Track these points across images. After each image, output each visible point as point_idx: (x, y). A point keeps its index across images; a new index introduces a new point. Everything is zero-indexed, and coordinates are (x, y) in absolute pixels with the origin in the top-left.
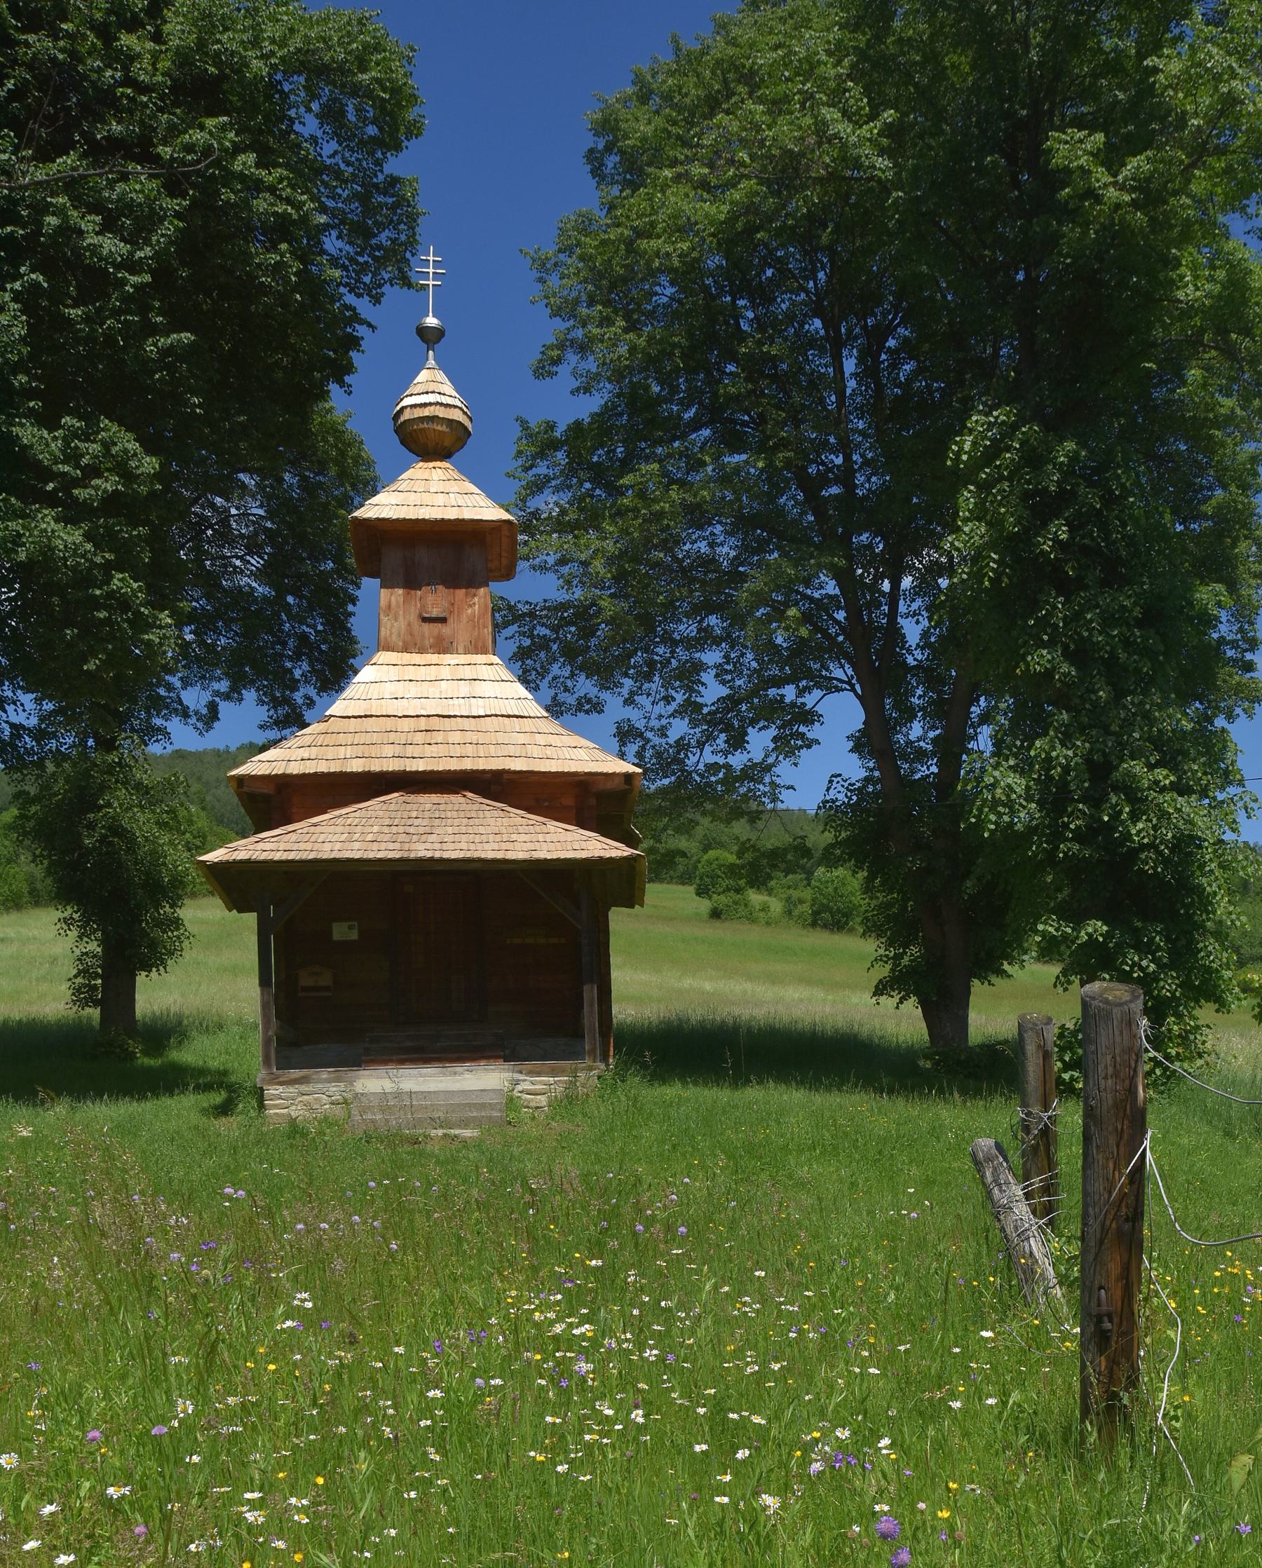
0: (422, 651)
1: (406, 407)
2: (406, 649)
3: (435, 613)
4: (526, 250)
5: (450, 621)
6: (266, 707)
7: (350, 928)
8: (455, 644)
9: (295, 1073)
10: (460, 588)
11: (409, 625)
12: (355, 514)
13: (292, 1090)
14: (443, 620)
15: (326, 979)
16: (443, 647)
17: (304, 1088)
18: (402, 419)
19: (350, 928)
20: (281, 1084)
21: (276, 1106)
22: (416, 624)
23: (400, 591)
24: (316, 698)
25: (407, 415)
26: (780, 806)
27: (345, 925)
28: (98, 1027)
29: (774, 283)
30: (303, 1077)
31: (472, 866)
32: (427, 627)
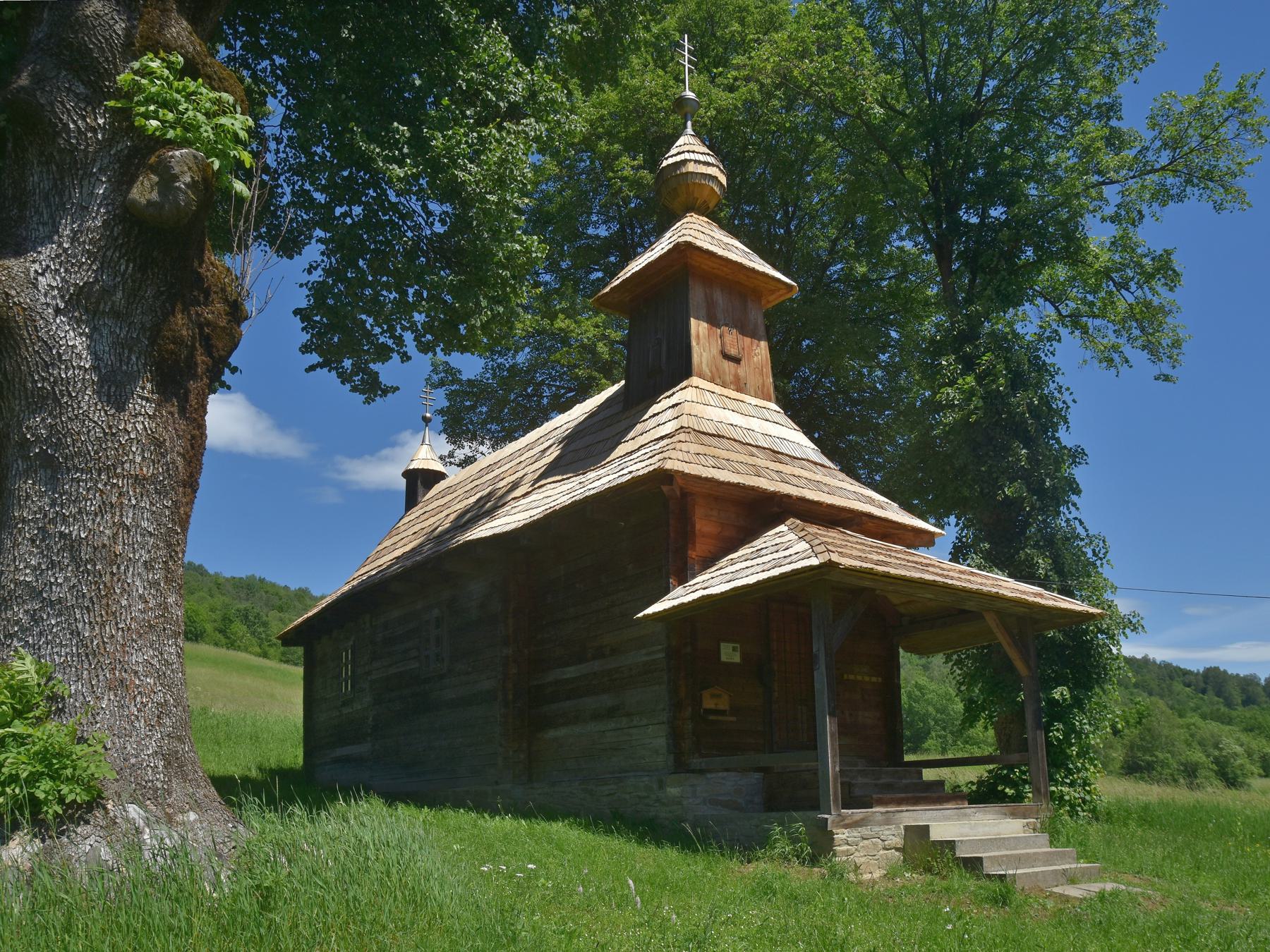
1: (690, 160)
2: (712, 381)
3: (733, 352)
5: (742, 362)
9: (858, 813)
14: (737, 360)
15: (723, 704)
17: (865, 831)
18: (684, 170)
19: (734, 649)
20: (846, 826)
23: (705, 325)
25: (691, 167)
30: (863, 819)
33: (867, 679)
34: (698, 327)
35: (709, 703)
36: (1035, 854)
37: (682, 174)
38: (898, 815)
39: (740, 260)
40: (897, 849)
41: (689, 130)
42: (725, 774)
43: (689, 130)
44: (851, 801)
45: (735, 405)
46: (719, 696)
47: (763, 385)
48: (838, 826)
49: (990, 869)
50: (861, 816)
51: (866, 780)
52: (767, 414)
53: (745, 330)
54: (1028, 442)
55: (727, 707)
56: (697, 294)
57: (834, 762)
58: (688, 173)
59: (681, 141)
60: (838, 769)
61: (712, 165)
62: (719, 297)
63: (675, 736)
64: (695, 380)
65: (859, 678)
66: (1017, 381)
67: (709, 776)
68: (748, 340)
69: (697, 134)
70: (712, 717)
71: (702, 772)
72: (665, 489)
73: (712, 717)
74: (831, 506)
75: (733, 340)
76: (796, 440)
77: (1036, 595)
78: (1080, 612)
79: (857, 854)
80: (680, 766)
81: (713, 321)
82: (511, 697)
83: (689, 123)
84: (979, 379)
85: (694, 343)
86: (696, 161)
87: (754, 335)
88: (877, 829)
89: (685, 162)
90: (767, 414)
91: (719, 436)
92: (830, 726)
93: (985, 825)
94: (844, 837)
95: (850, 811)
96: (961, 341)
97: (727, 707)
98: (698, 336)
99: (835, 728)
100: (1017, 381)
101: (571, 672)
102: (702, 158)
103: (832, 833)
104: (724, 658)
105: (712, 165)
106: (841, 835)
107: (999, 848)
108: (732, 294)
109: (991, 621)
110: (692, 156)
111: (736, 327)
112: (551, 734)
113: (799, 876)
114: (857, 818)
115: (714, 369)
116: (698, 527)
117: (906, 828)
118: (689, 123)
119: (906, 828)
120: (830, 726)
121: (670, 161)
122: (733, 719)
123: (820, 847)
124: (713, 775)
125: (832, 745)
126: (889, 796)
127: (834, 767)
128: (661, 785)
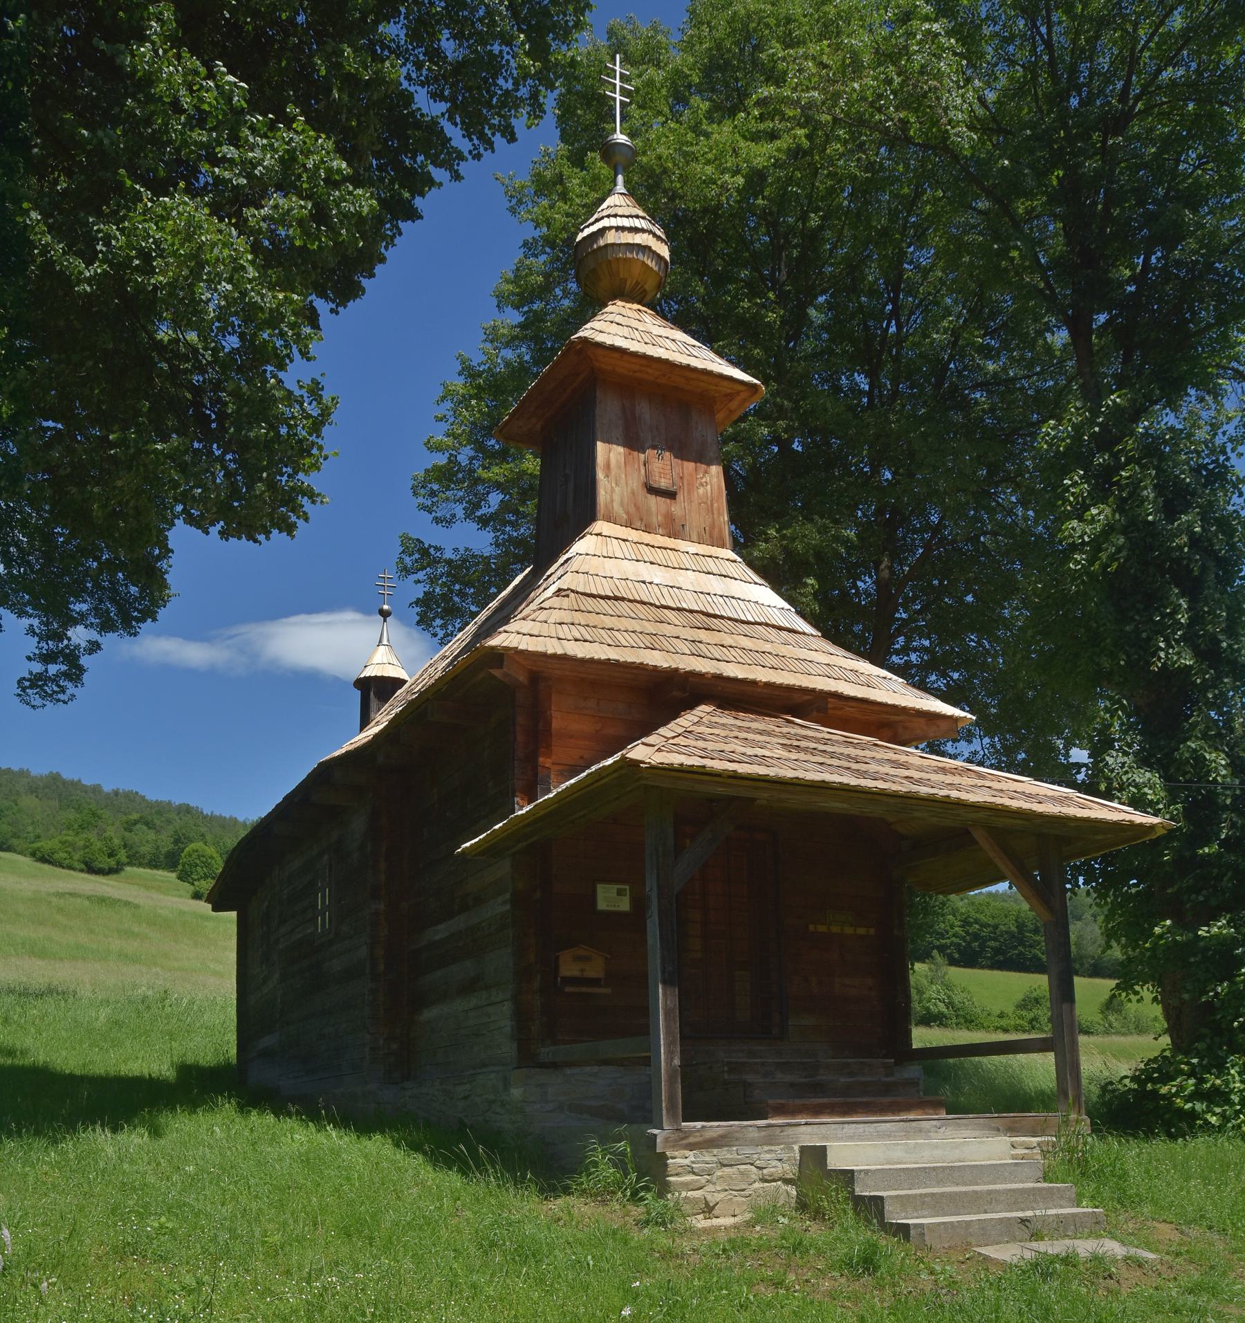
0: (648, 530)
1: (610, 228)
2: (629, 524)
3: (664, 483)
4: (499, 175)
5: (680, 497)
6: (36, 639)
7: (620, 893)
8: (687, 528)
9: (716, 1128)
10: (689, 460)
11: (633, 493)
12: (581, 334)
13: (708, 1157)
14: (671, 495)
15: (595, 969)
16: (674, 529)
17: (725, 1154)
18: (602, 243)
19: (620, 893)
20: (691, 1147)
21: (687, 1186)
22: (642, 493)
23: (621, 449)
24: (100, 640)
25: (611, 237)
26: (1071, 760)
27: (614, 888)
28: (235, 1062)
29: (1145, 166)
30: (723, 1137)
31: (837, 806)
32: (653, 501)
33: (849, 930)
34: (609, 455)
35: (569, 968)
36: (990, 1192)
37: (600, 248)
38: (790, 1131)
39: (685, 360)
40: (787, 1182)
41: (620, 188)
42: (596, 1069)
43: (620, 188)
44: (700, 1105)
45: (659, 556)
46: (586, 959)
47: (713, 526)
48: (677, 1145)
49: (895, 1216)
50: (720, 1131)
51: (788, 1078)
52: (711, 565)
53: (684, 449)
54: (1193, 590)
55: (602, 975)
56: (608, 408)
57: (670, 1053)
58: (607, 246)
59: (610, 201)
60: (677, 1062)
61: (643, 231)
62: (645, 410)
63: (521, 1017)
64: (600, 526)
65: (835, 929)
66: (1175, 499)
67: (568, 1071)
68: (690, 466)
69: (631, 192)
70: (568, 989)
71: (554, 1066)
72: (496, 673)
73: (568, 989)
74: (769, 685)
75: (664, 467)
76: (764, 599)
77: (1054, 799)
78: (1116, 824)
79: (710, 1188)
80: (527, 1058)
81: (633, 443)
82: (382, 967)
83: (620, 178)
84: (1121, 507)
85: (600, 475)
86: (618, 228)
87: (701, 457)
88: (748, 1150)
89: (603, 231)
90: (711, 565)
91: (616, 598)
92: (663, 999)
93: (936, 1147)
94: (687, 1162)
95: (699, 1124)
96: (1100, 455)
97: (602, 975)
98: (608, 466)
99: (674, 1002)
100: (1175, 499)
101: (441, 931)
102: (626, 223)
103: (663, 1157)
104: (602, 905)
105: (643, 231)
106: (679, 1159)
107: (940, 1182)
108: (664, 407)
109: (978, 835)
110: (613, 222)
111: (670, 449)
112: (428, 1014)
113: (616, 1214)
114: (709, 1134)
115: (632, 510)
116: (555, 725)
117: (803, 1149)
118: (620, 178)
119: (803, 1149)
120: (663, 999)
121: (587, 232)
122: (607, 991)
123: (650, 1171)
124: (577, 1070)
125: (667, 1027)
126: (798, 1102)
127: (670, 1059)
128: (507, 1084)
